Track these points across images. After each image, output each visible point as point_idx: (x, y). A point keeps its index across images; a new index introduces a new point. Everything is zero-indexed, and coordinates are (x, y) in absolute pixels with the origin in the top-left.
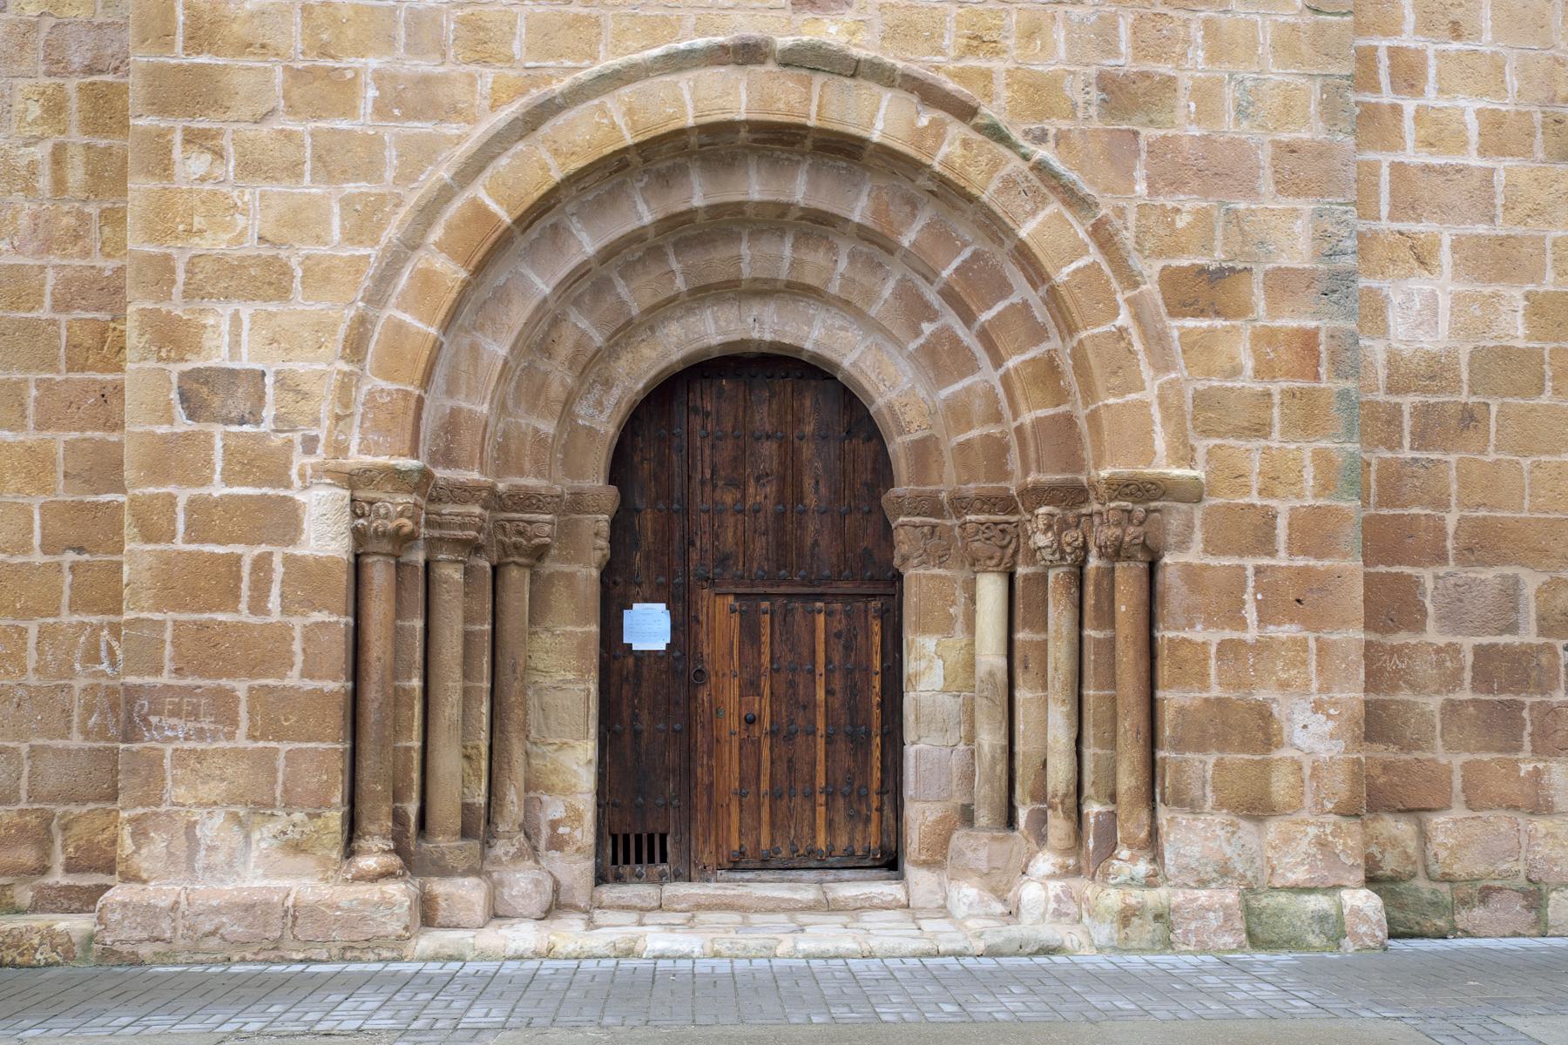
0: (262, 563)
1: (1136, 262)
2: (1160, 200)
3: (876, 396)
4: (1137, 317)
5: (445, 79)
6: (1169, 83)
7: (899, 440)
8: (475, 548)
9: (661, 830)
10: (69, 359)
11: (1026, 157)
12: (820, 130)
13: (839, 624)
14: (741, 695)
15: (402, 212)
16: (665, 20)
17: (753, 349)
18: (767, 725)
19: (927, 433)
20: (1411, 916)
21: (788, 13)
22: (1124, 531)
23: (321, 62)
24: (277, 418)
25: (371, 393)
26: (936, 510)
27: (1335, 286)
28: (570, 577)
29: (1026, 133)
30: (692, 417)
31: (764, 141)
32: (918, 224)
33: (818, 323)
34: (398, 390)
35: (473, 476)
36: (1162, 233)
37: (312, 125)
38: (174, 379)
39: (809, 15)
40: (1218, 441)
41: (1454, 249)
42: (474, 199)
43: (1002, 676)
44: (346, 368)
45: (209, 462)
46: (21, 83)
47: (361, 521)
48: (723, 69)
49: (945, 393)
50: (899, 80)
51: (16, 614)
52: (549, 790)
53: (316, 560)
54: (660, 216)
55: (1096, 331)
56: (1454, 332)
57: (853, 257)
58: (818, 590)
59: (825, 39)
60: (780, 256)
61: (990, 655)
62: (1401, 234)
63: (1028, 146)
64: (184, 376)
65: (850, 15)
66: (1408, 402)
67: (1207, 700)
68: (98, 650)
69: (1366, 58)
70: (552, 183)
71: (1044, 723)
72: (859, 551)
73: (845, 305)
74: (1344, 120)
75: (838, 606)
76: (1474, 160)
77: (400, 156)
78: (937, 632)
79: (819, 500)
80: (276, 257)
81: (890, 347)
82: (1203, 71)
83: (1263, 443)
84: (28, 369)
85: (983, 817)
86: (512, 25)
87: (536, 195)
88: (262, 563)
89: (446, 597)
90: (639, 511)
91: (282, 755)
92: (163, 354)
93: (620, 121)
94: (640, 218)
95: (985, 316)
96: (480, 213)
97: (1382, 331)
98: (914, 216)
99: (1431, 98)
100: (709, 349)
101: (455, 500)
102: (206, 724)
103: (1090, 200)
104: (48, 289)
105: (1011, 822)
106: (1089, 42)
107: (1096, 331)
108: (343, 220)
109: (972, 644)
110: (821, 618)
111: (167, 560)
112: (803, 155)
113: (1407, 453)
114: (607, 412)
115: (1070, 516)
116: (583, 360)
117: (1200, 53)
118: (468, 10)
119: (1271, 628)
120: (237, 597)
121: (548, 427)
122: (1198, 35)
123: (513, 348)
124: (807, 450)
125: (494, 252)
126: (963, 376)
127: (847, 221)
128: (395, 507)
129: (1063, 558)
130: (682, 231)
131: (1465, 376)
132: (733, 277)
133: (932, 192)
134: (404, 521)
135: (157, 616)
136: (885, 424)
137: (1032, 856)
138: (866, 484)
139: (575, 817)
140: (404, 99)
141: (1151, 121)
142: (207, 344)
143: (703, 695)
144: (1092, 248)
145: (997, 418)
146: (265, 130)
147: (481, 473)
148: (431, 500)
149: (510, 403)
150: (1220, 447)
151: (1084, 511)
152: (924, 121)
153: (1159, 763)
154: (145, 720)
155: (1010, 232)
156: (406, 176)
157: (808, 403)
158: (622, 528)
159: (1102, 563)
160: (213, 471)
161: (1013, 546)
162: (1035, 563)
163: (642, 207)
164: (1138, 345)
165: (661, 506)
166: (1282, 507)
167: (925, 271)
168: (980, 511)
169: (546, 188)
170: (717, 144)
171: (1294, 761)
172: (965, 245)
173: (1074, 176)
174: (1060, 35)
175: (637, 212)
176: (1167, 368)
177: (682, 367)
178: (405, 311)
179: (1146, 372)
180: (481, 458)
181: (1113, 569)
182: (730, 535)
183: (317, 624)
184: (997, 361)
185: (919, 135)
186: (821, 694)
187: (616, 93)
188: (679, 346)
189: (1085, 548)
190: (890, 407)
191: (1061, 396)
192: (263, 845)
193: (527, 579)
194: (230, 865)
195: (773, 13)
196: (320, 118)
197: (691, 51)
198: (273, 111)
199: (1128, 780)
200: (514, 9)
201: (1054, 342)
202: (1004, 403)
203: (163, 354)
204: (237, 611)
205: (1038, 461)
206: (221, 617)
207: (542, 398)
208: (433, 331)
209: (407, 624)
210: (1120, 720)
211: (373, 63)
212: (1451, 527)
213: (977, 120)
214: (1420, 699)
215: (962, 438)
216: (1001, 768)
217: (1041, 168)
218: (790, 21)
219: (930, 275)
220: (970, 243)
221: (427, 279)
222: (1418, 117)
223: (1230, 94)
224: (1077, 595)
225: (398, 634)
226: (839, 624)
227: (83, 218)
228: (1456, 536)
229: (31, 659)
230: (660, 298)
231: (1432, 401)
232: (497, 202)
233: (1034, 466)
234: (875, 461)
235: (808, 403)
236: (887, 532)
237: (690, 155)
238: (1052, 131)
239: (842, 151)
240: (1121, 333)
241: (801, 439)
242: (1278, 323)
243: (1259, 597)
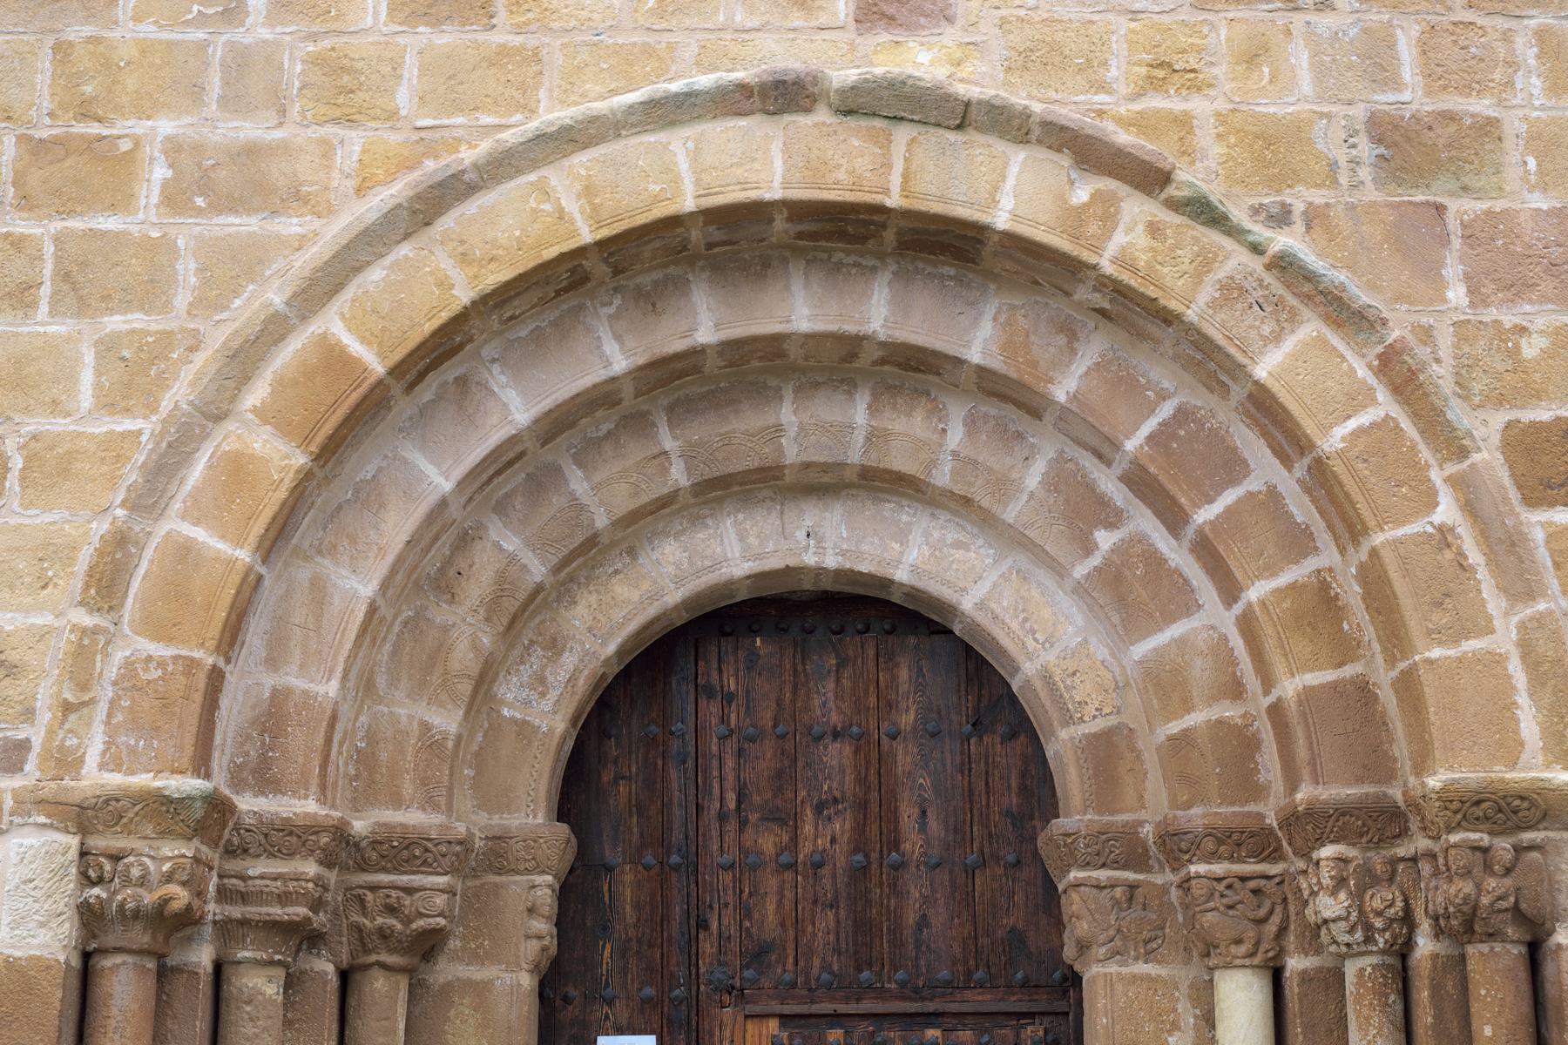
1: (1459, 415)
2: (1491, 314)
3: (1020, 658)
4: (1470, 508)
5: (284, 148)
6: (1488, 128)
7: (1064, 734)
8: (307, 938)
11: (1256, 249)
12: (907, 214)
15: (200, 359)
16: (648, 51)
17: (808, 585)
19: (1113, 721)
21: (850, 35)
22: (1478, 886)
23: (81, 128)
25: (128, 664)
26: (1136, 857)
28: (481, 989)
29: (1256, 211)
30: (703, 702)
31: (814, 236)
32: (1081, 366)
33: (916, 537)
34: (176, 658)
35: (306, 807)
36: (1500, 367)
37: (57, 225)
39: (884, 37)
42: (324, 337)
44: (88, 620)
47: (96, 891)
48: (742, 122)
49: (1141, 649)
50: (1036, 132)
54: (641, 361)
55: (1400, 532)
57: (971, 424)
58: (931, 1007)
59: (910, 70)
60: (851, 424)
65: (951, 36)
70: (455, 308)
72: (1000, 933)
73: (960, 505)
77: (200, 271)
79: (927, 842)
81: (1042, 575)
82: (1542, 108)
86: (397, 65)
87: (429, 327)
89: (249, 1030)
90: (609, 869)
93: (571, 206)
94: (608, 364)
95: (1204, 515)
96: (333, 358)
98: (1074, 352)
100: (730, 585)
101: (273, 851)
103: (1370, 314)
106: (1350, 67)
107: (1400, 532)
108: (98, 373)
112: (881, 256)
114: (553, 695)
115: (1377, 860)
116: (511, 605)
117: (1534, 80)
118: (327, 43)
121: (447, 721)
122: (1530, 55)
123: (384, 586)
124: (904, 757)
125: (351, 427)
126: (1170, 618)
127: (958, 362)
128: (159, 864)
129: (1368, 940)
130: (676, 383)
132: (768, 462)
133: (1102, 312)
134: (174, 889)
136: (1039, 706)
138: (1008, 813)
140: (206, 182)
141: (1465, 189)
144: (1382, 395)
145: (1236, 690)
147: (322, 800)
148: (230, 852)
149: (381, 681)
151: (1401, 852)
152: (1081, 195)
155: (1238, 371)
156: (209, 301)
157: (904, 674)
158: (578, 898)
159: (1442, 948)
161: (1276, 919)
162: (1318, 950)
163: (611, 347)
164: (1475, 557)
165: (649, 859)
167: (1095, 441)
168: (1213, 857)
169: (445, 316)
170: (736, 240)
172: (1163, 396)
173: (1341, 276)
174: (1300, 58)
175: (602, 355)
176: (1530, 593)
177: (685, 617)
178: (197, 523)
179: (1494, 603)
180: (323, 774)
181: (1463, 958)
182: (771, 908)
184: (1230, 590)
185: (1075, 218)
187: (566, 162)
188: (678, 581)
189: (1408, 919)
190: (1047, 678)
191: (1346, 649)
193: (403, 994)
195: (826, 35)
196: (71, 213)
197: (689, 95)
200: (401, 40)
201: (1327, 556)
202: (1246, 665)
205: (1312, 763)
207: (438, 671)
208: (244, 555)
211: (166, 126)
213: (1171, 191)
215: (1174, 727)
217: (1284, 265)
218: (852, 46)
219: (1105, 449)
220: (1171, 392)
221: (237, 470)
224: (1399, 1007)
230: (644, 499)
232: (363, 340)
233: (1306, 772)
234: (1024, 774)
235: (904, 674)
236: (1049, 898)
237: (692, 261)
238: (1299, 207)
239: (946, 248)
240: (1444, 534)
241: (893, 737)
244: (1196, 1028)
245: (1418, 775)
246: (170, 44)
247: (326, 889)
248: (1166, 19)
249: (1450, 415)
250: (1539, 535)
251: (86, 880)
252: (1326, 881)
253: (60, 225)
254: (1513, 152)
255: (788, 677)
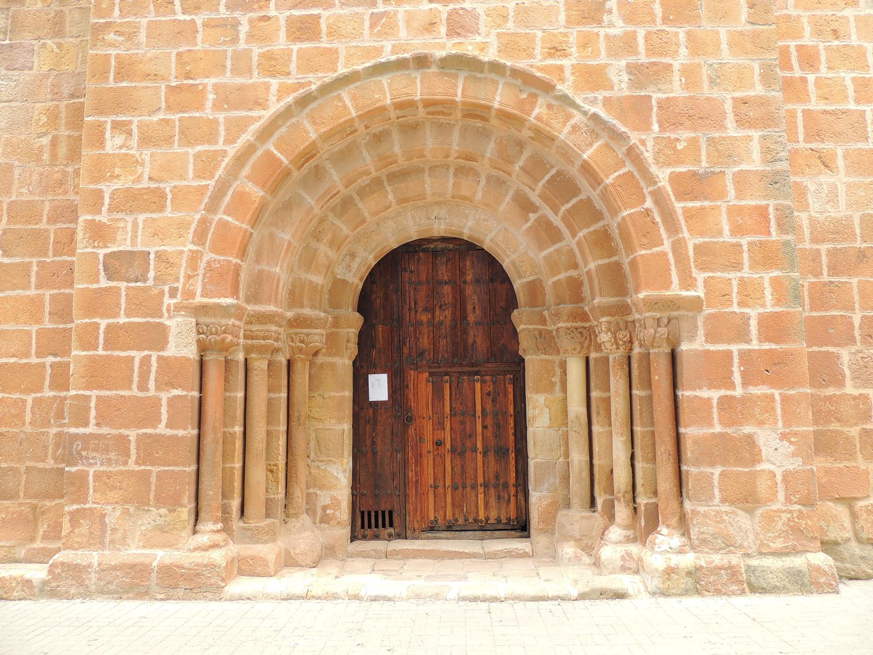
0: (145, 362)
1: (654, 169)
4: (657, 202)
9: (389, 508)
10: (54, 249)
11: (585, 113)
13: (490, 388)
14: (433, 429)
15: (227, 160)
18: (448, 446)
20: (849, 566)
23: (186, 82)
24: (155, 278)
25: (208, 262)
27: (774, 181)
28: (333, 365)
36: (669, 153)
38: (101, 258)
40: (711, 274)
41: (845, 157)
43: (584, 418)
44: (195, 248)
45: (118, 304)
46: (38, 105)
50: (508, 73)
51: (21, 392)
52: (322, 487)
53: (176, 358)
56: (849, 206)
61: (576, 407)
62: (811, 149)
63: (587, 107)
64: (105, 255)
66: (824, 248)
67: (713, 433)
68: (63, 412)
69: (784, 53)
71: (610, 446)
74: (775, 84)
75: (487, 378)
76: (852, 106)
78: (545, 392)
80: (158, 188)
83: (739, 274)
84: (33, 256)
85: (576, 502)
88: (145, 362)
89: (256, 379)
91: (154, 475)
92: (96, 244)
97: (806, 207)
99: (824, 72)
102: (112, 455)
104: (45, 212)
105: (593, 503)
108: (195, 166)
109: (566, 398)
110: (478, 386)
111: (92, 360)
113: (825, 278)
119: (751, 387)
120: (131, 382)
124: (469, 290)
131: (858, 231)
135: (88, 393)
137: (606, 528)
139: (336, 504)
140: (228, 99)
141: (659, 90)
142: (119, 237)
143: (411, 431)
145: (575, 266)
146: (155, 119)
149: (296, 267)
150: (712, 278)
153: (684, 474)
154: (79, 453)
157: (468, 263)
160: (120, 309)
164: (658, 219)
166: (753, 313)
171: (771, 472)
183: (175, 397)
186: (479, 428)
192: (143, 528)
194: (124, 538)
198: (159, 109)
199: (666, 484)
203: (96, 244)
204: (131, 389)
206: (122, 393)
209: (232, 395)
210: (657, 446)
212: (857, 322)
214: (845, 429)
215: (555, 279)
216: (586, 474)
217: (595, 117)
221: (241, 198)
222: (818, 83)
223: (705, 72)
224: (627, 369)
225: (227, 402)
226: (490, 388)
227: (65, 174)
228: (861, 327)
229: (28, 418)
231: (839, 247)
233: (598, 293)
242: (743, 203)
243: (742, 369)
244: (561, 375)
245: (636, 294)
246: (214, 51)
247: (280, 334)
248: (555, 31)
249: (651, 170)
250: (679, 212)
251: (199, 333)
252: (604, 329)
253: (180, 115)
254: (676, 76)
255: (431, 265)
